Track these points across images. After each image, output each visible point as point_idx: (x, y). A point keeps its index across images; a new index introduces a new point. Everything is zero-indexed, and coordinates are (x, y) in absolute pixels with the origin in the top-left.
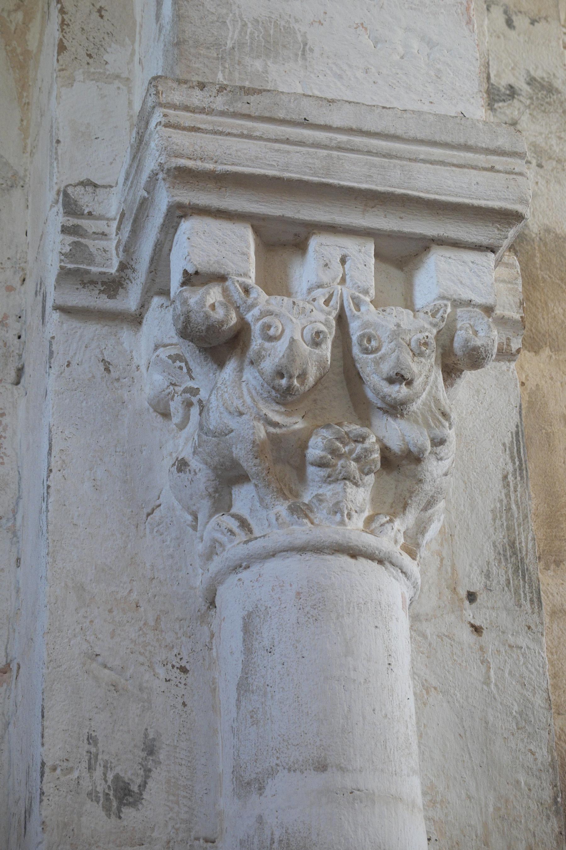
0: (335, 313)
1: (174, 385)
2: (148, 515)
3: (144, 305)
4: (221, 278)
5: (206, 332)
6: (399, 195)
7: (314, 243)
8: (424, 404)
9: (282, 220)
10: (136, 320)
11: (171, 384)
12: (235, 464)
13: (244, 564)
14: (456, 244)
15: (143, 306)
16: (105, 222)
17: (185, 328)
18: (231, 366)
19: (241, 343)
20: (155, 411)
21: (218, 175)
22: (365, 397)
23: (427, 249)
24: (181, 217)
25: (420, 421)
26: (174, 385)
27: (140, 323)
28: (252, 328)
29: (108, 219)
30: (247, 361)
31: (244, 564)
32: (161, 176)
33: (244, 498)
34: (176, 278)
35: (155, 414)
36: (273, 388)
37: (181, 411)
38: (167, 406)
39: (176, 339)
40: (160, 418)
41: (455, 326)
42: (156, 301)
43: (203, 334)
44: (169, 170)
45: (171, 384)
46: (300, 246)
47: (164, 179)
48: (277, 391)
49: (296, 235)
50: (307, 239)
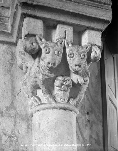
0: (63, 47)
1: (24, 62)
2: (18, 94)
3: (17, 41)
4: (35, 36)
5: (31, 50)
6: (88, 16)
7: (58, 26)
8: (83, 71)
9: (50, 19)
10: (15, 44)
11: (23, 62)
12: (38, 85)
13: (39, 110)
14: (93, 29)
15: (17, 41)
16: (8, 18)
17: (25, 49)
18: (37, 60)
19: (39, 54)
20: (20, 68)
21: (34, 5)
22: (69, 68)
23: (85, 30)
24: (25, 17)
25: (82, 75)
26: (24, 62)
27: (17, 45)
28: (42, 50)
29: (8, 18)
30: (41, 59)
31: (39, 110)
32: (19, 5)
33: (39, 93)
34: (23, 35)
35: (20, 69)
36: (47, 66)
37: (25, 69)
38: (22, 67)
39: (24, 51)
40: (21, 70)
41: (91, 51)
42: (20, 40)
43: (30, 51)
44: (21, 3)
45: (23, 62)
46: (55, 27)
47: (20, 6)
48: (48, 67)
49: (54, 24)
50: (57, 25)
